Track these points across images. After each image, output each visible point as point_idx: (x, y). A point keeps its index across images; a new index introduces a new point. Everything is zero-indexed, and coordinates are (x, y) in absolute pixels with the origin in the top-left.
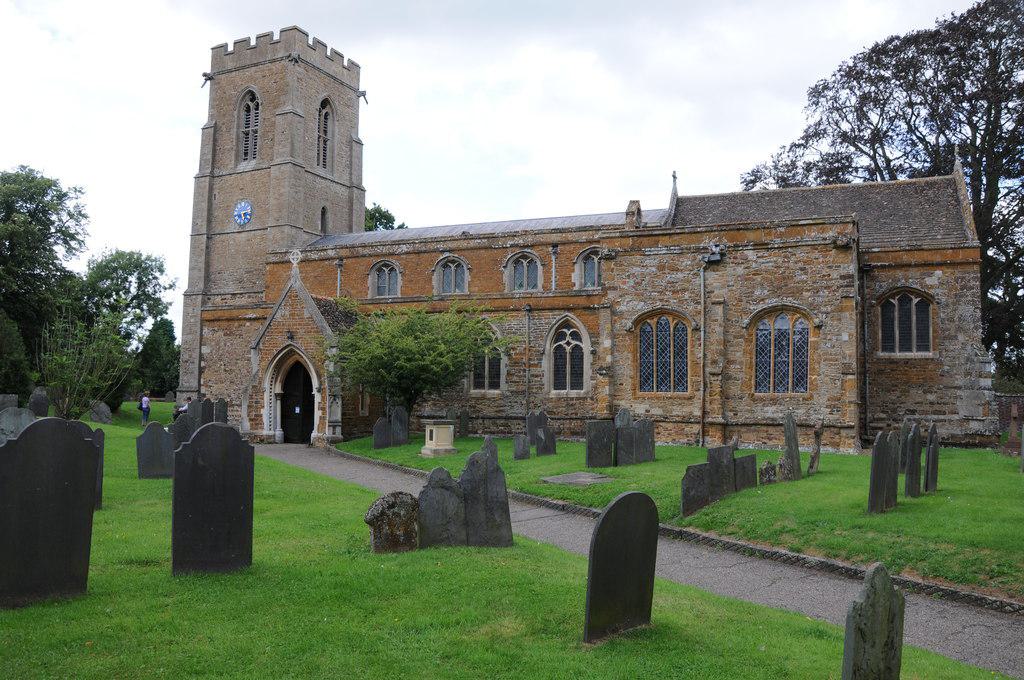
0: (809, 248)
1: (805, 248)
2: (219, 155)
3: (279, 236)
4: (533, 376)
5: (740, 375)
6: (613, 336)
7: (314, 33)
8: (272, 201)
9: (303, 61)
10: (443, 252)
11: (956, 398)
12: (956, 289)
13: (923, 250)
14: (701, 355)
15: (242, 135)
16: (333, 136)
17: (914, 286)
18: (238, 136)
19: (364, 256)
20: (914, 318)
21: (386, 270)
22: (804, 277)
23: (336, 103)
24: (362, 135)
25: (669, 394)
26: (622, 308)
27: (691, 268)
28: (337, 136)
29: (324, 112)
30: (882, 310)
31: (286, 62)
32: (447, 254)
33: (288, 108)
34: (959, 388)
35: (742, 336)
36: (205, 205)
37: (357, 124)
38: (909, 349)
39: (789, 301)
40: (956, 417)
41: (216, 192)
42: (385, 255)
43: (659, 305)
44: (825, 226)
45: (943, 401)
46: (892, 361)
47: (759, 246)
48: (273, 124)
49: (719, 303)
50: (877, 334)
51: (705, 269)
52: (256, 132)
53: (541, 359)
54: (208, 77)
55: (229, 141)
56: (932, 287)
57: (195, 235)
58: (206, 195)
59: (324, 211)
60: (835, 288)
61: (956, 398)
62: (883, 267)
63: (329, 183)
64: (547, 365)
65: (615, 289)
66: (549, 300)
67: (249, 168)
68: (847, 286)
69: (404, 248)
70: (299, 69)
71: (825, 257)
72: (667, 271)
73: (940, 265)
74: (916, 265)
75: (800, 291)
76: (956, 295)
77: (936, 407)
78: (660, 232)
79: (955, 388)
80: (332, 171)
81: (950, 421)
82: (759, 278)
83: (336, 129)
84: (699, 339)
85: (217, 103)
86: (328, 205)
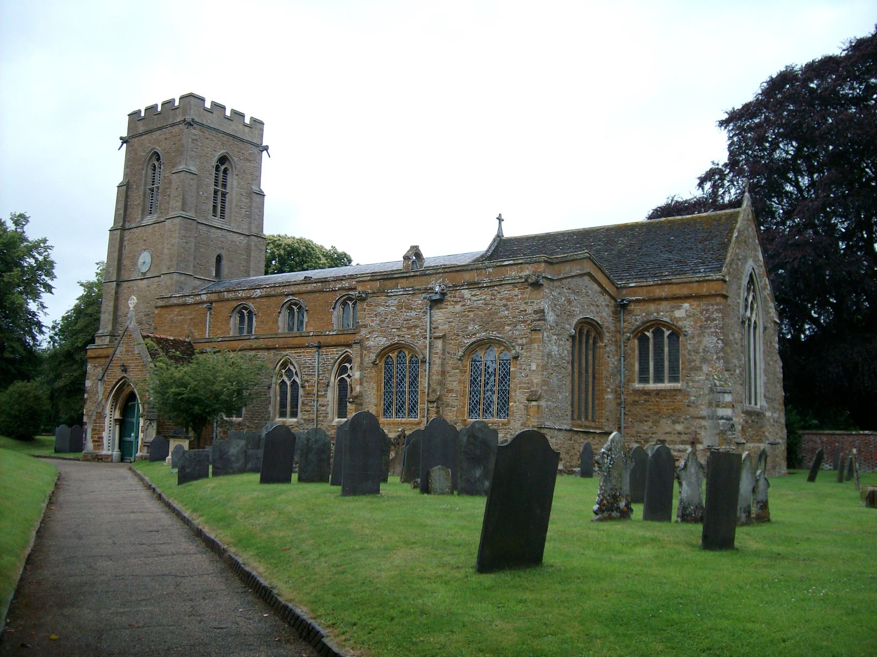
1: (507, 286)
2: (129, 211)
3: (169, 282)
4: (320, 405)
5: (456, 403)
6: (362, 368)
7: (142, 106)
8: (166, 251)
9: (197, 123)
10: (287, 295)
11: (701, 427)
14: (426, 385)
16: (232, 188)
17: (665, 319)
18: (145, 193)
19: (228, 300)
20: (666, 350)
24: (264, 186)
25: (404, 420)
26: (371, 343)
27: (421, 307)
29: (223, 168)
30: (639, 342)
31: (182, 126)
32: (291, 297)
33: (181, 167)
34: (703, 418)
36: (116, 255)
39: (494, 334)
41: (125, 243)
42: (243, 299)
44: (523, 266)
48: (170, 182)
50: (633, 365)
52: (158, 188)
53: (327, 391)
54: (124, 140)
55: (137, 198)
58: (117, 246)
59: (219, 259)
60: (529, 322)
61: (701, 427)
62: (638, 301)
63: (224, 233)
65: (365, 326)
66: (335, 338)
68: (539, 320)
69: (258, 292)
70: (195, 131)
72: (404, 310)
73: (687, 298)
74: (666, 299)
75: (503, 325)
76: (701, 327)
78: (400, 275)
82: (472, 315)
84: (425, 370)
86: (223, 253)
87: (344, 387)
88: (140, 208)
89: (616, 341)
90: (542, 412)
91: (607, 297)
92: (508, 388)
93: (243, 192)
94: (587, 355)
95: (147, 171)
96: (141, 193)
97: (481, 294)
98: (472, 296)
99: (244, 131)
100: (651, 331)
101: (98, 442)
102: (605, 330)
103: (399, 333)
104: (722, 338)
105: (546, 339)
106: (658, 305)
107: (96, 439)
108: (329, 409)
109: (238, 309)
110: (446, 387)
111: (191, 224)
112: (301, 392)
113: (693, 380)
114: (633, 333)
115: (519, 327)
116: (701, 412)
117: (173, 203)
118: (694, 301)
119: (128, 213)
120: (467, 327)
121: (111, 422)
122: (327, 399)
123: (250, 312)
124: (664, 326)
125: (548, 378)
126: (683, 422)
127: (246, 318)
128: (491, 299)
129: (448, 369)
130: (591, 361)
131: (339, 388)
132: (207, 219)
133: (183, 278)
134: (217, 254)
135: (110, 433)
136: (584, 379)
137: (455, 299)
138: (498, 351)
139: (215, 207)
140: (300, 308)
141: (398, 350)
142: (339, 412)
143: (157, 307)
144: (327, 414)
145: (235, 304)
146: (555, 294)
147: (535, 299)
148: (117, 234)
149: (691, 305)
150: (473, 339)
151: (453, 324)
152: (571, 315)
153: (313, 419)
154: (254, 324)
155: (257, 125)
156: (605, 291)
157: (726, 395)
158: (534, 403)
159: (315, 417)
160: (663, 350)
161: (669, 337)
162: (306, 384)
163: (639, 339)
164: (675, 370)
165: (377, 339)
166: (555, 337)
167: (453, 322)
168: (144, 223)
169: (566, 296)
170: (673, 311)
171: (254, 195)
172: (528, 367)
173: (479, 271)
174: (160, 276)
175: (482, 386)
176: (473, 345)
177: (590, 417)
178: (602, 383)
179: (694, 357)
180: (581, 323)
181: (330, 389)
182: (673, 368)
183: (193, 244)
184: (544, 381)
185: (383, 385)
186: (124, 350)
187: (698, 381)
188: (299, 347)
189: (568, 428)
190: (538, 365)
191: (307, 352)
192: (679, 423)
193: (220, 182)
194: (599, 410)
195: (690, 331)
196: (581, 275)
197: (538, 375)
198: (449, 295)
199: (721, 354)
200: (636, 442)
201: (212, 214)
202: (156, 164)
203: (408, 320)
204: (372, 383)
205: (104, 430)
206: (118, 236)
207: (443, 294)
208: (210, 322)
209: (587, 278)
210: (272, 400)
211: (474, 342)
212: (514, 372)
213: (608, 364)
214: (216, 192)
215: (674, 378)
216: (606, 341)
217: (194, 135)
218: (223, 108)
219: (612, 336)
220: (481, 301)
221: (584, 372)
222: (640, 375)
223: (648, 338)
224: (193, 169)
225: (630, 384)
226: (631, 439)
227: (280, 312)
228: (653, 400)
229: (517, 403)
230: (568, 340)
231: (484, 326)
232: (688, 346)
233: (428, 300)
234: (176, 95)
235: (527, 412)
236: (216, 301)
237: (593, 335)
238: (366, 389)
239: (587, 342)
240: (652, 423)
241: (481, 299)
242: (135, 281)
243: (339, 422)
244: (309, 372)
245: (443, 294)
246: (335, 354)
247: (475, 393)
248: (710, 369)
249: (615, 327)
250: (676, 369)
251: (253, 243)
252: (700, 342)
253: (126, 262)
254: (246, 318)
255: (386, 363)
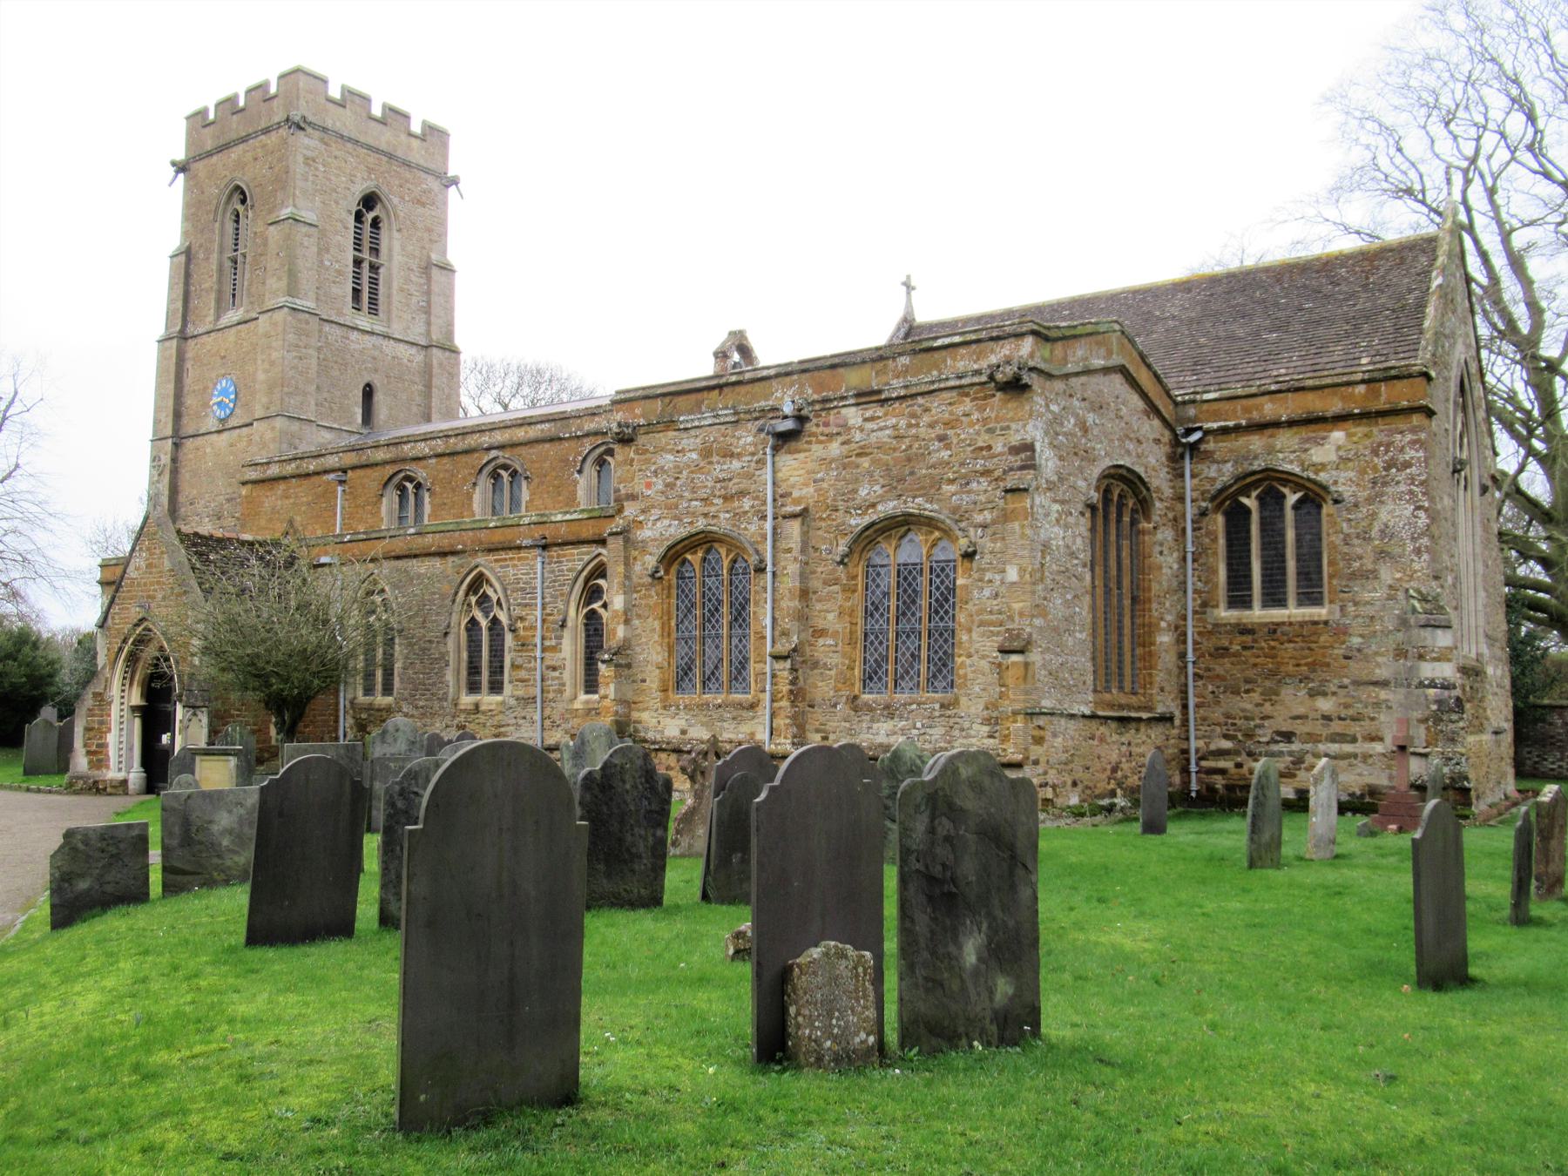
0: (954, 393)
1: (945, 395)
3: (269, 435)
4: (548, 668)
6: (629, 588)
10: (489, 449)
11: (1377, 705)
12: (1375, 468)
13: (1303, 389)
15: (228, 264)
17: (1288, 467)
20: (1290, 535)
21: (409, 486)
22: (945, 454)
23: (396, 202)
24: (453, 256)
26: (645, 534)
27: (752, 449)
28: (398, 258)
29: (370, 216)
32: (493, 453)
33: (286, 212)
34: (1384, 684)
35: (836, 582)
36: (171, 386)
37: (443, 235)
38: (1281, 602)
40: (1378, 748)
41: (188, 365)
43: (701, 524)
44: (983, 345)
45: (1351, 712)
46: (1245, 630)
47: (866, 396)
49: (794, 516)
50: (1215, 572)
51: (776, 449)
54: (181, 168)
55: (207, 278)
56: (1322, 467)
57: (157, 439)
59: (368, 393)
62: (1224, 431)
63: (380, 341)
64: (455, 649)
65: (633, 497)
67: (235, 319)
68: (1022, 468)
71: (982, 409)
72: (715, 459)
73: (1340, 419)
74: (1291, 423)
75: (937, 484)
77: (1336, 727)
79: (1375, 683)
80: (389, 320)
81: (1366, 757)
82: (865, 463)
83: (396, 249)
85: (194, 211)
87: (596, 630)
88: (213, 296)
89: (1175, 519)
90: (1033, 677)
91: (1156, 422)
92: (950, 624)
93: (414, 265)
94: (1119, 550)
95: (223, 223)
96: (214, 268)
97: (886, 414)
98: (866, 420)
99: (409, 147)
100: (1254, 494)
101: (98, 756)
102: (1154, 495)
103: (706, 510)
104: (1426, 504)
105: (1040, 510)
106: (1271, 436)
107: (94, 748)
108: (567, 676)
109: (396, 480)
110: (811, 623)
111: (307, 323)
112: (509, 639)
113: (1357, 599)
114: (1213, 499)
115: (974, 485)
116: (1377, 671)
117: (273, 283)
118: (1359, 425)
119: (191, 306)
120: (855, 491)
121: (125, 713)
122: (562, 655)
123: (418, 486)
124: (1285, 482)
125: (1045, 599)
126: (1334, 694)
127: (412, 498)
128: (910, 426)
129: (815, 583)
130: (1126, 562)
131: (587, 630)
132: (340, 313)
133: (295, 426)
134: (365, 381)
135: (121, 736)
136: (1115, 601)
137: (826, 430)
138: (927, 541)
139: (356, 293)
140: (514, 474)
141: (705, 546)
142: (586, 681)
143: (244, 483)
144: (564, 685)
145: (390, 470)
146: (1054, 408)
147: (1012, 420)
148: (171, 348)
149: (1349, 435)
150: (867, 520)
151: (825, 485)
152: (1088, 456)
153: (534, 698)
154: (427, 509)
155: (435, 136)
156: (1152, 409)
157: (1439, 632)
158: (1015, 658)
159: (538, 691)
160: (1282, 534)
161: (1297, 507)
162: (520, 625)
163: (1227, 514)
164: (1311, 580)
165: (658, 524)
166: (1056, 507)
167: (823, 480)
168: (224, 321)
169: (1076, 416)
170: (1306, 450)
171: (435, 271)
172: (998, 577)
173: (879, 365)
174: (251, 424)
175: (893, 621)
176: (871, 530)
177: (1127, 685)
178: (1150, 610)
179: (1359, 551)
180: (1105, 477)
181: (567, 634)
182: (1308, 573)
183: (314, 361)
184: (1037, 606)
185: (673, 623)
186: (143, 564)
187: (1368, 603)
188: (503, 549)
189: (1087, 712)
190: (1022, 570)
191: (519, 559)
192: (1324, 694)
193: (366, 245)
194: (1145, 668)
195: (1346, 490)
196: (1106, 370)
197: (1024, 593)
198: (815, 421)
199: (1425, 541)
200: (1226, 737)
201: (351, 305)
202: (240, 208)
203: (724, 480)
204: (650, 619)
205: (109, 730)
206: (174, 352)
207: (801, 419)
208: (343, 508)
209: (1117, 379)
210: (452, 658)
211: (873, 524)
212: (965, 587)
213: (1160, 568)
214: (358, 262)
215: (1310, 596)
216: (1155, 518)
217: (307, 148)
218: (366, 100)
219: (1167, 508)
220: (887, 432)
221: (1113, 585)
222: (1229, 590)
223: (1248, 511)
224: (310, 217)
225: (1208, 610)
226: (1213, 731)
227: (475, 484)
228: (1263, 644)
229: (975, 658)
230: (1082, 514)
231: (896, 484)
232: (1345, 525)
233: (768, 433)
234: (269, 72)
235: (1001, 678)
236: (354, 468)
237: (1130, 505)
238: (639, 631)
239: (1119, 520)
240: (1262, 694)
241: (886, 427)
242: (206, 437)
243: (587, 702)
244: (525, 598)
245: (801, 419)
246: (577, 560)
247: (877, 637)
248: (1398, 575)
249: (1173, 487)
250: (1314, 576)
251: (435, 362)
252: (1373, 516)
253: (190, 401)
254: (412, 498)
255: (680, 576)
